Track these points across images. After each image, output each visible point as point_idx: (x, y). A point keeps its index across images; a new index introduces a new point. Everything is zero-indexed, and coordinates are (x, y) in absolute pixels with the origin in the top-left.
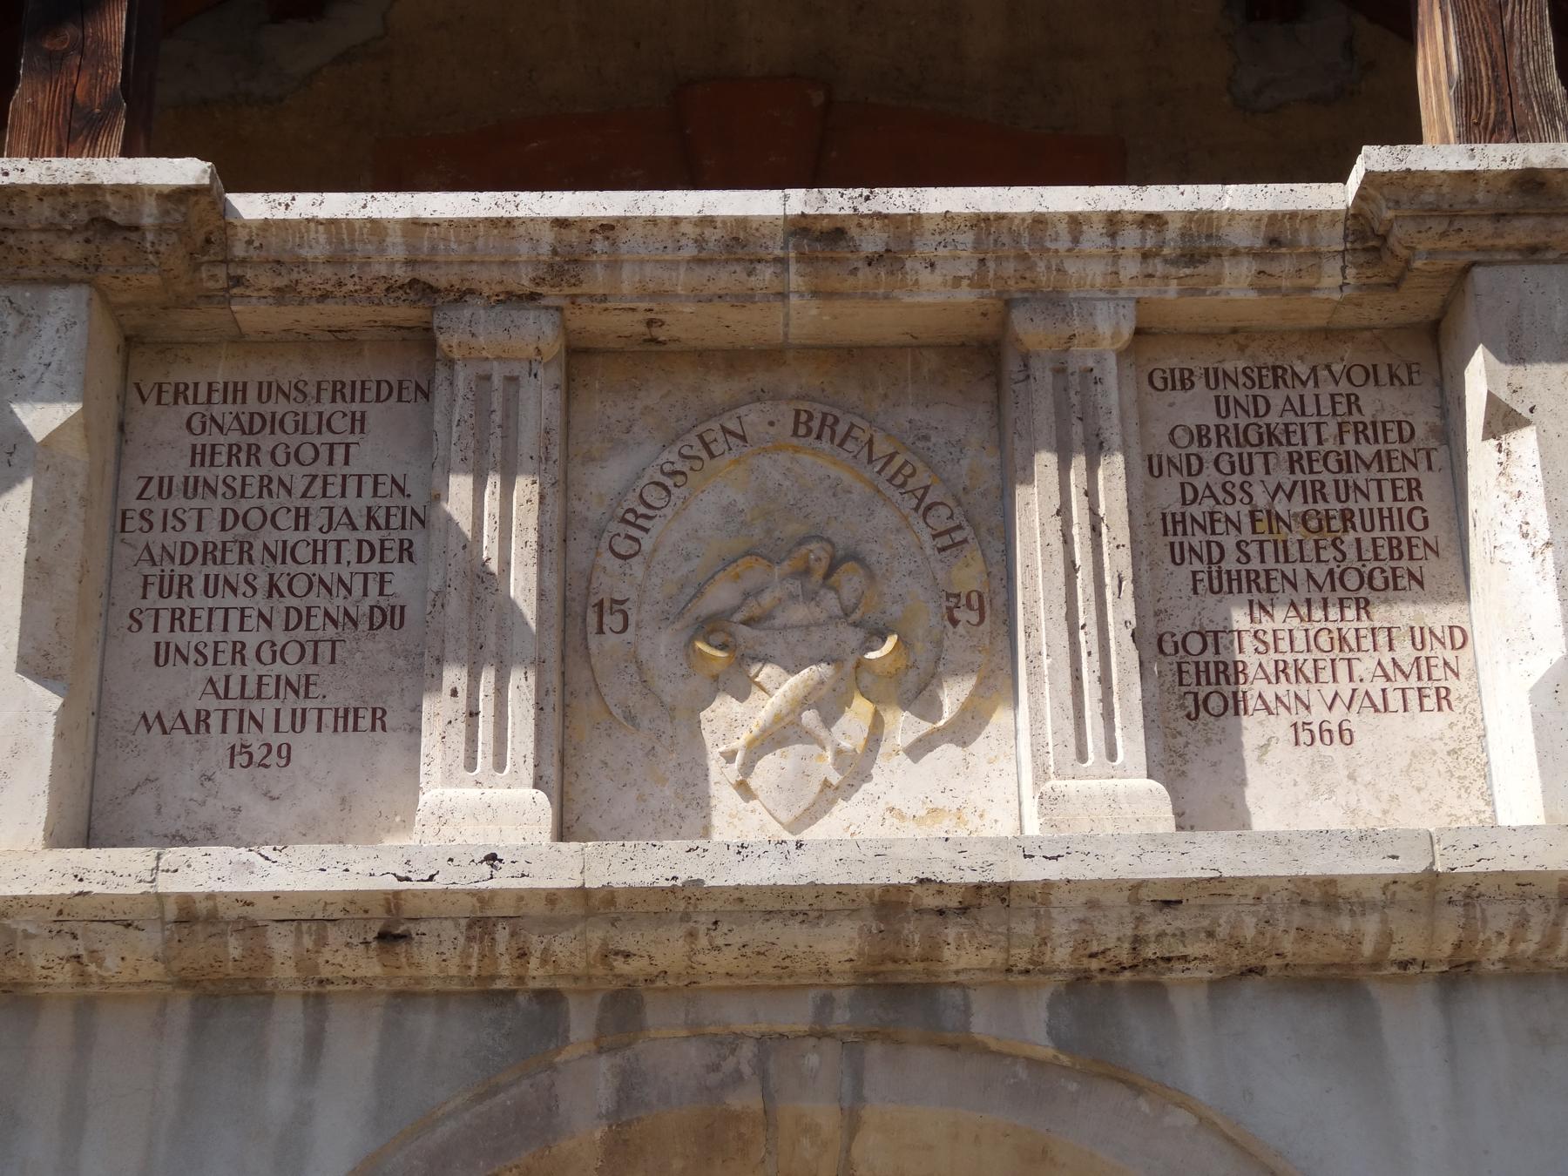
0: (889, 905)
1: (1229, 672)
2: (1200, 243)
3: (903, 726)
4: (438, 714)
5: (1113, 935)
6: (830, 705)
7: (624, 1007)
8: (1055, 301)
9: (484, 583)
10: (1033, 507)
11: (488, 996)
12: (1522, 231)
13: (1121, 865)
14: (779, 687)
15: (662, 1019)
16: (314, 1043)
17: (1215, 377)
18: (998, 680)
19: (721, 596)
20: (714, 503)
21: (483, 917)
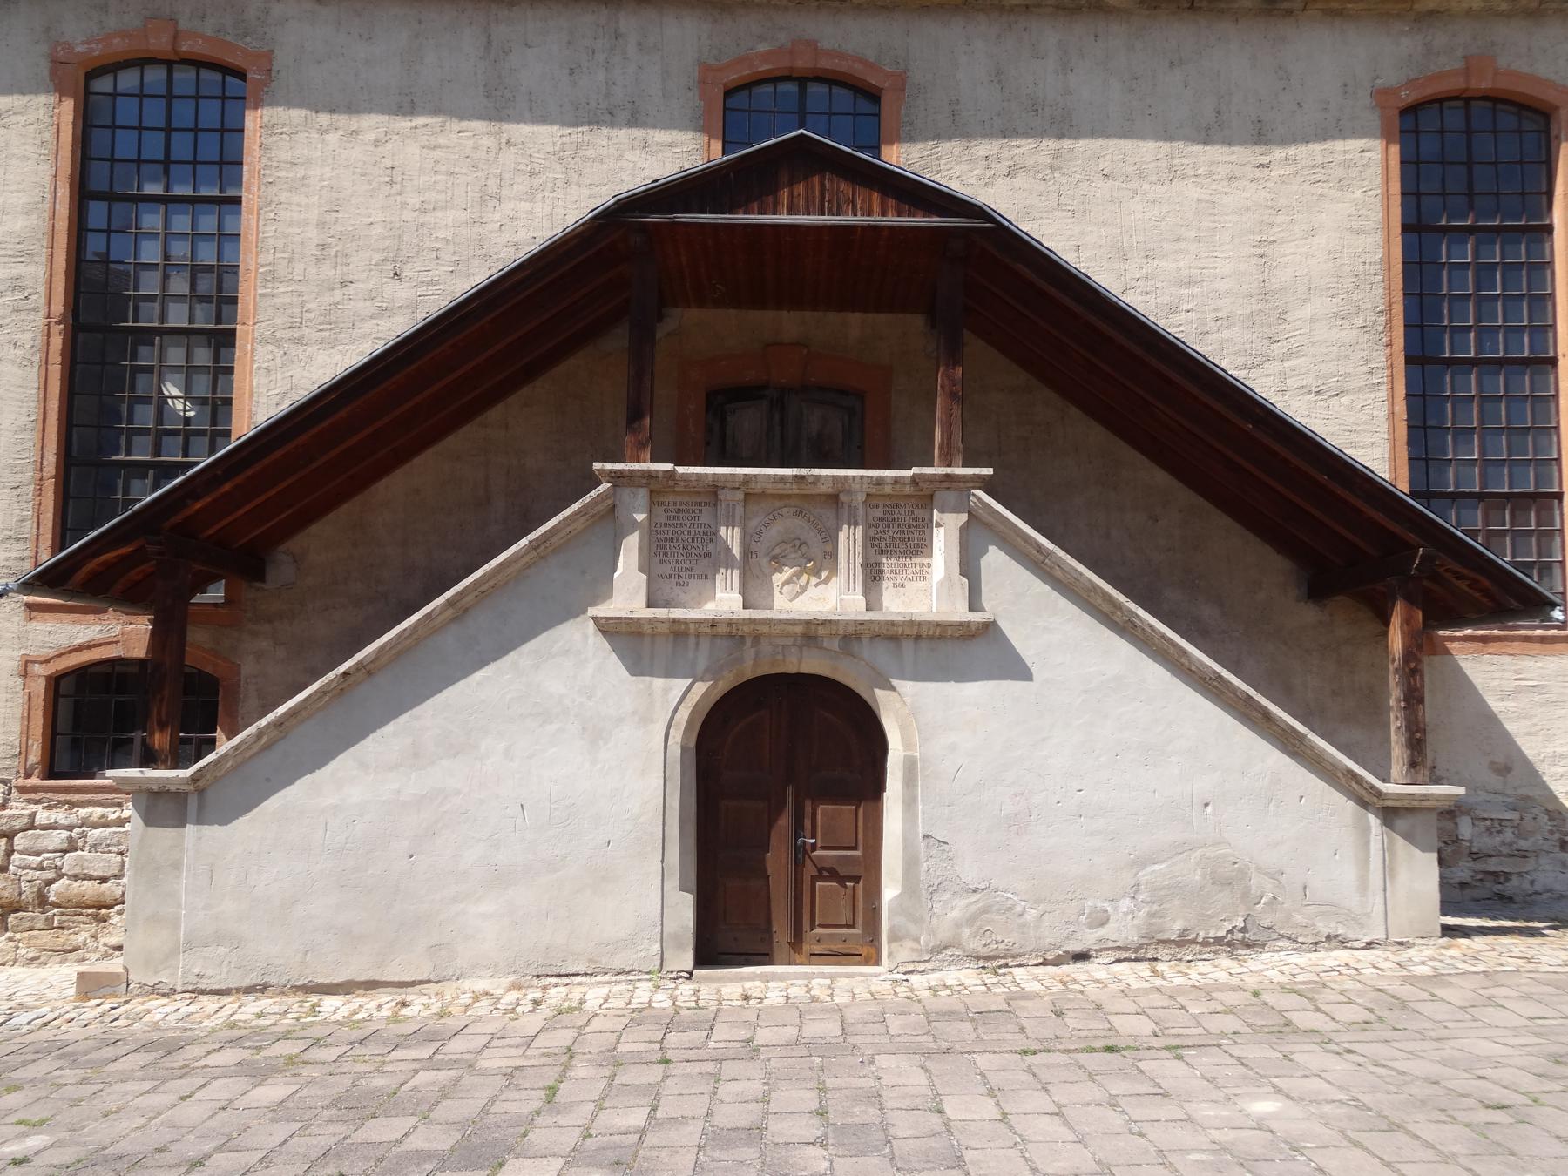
0: (808, 623)
1: (881, 572)
2: (880, 481)
3: (814, 580)
4: (719, 578)
5: (851, 629)
6: (798, 575)
8: (849, 492)
9: (729, 550)
10: (842, 536)
11: (730, 636)
12: (946, 485)
13: (852, 617)
14: (788, 572)
15: (764, 642)
16: (697, 644)
17: (884, 506)
18: (834, 570)
19: (777, 551)
20: (775, 531)
21: (730, 623)
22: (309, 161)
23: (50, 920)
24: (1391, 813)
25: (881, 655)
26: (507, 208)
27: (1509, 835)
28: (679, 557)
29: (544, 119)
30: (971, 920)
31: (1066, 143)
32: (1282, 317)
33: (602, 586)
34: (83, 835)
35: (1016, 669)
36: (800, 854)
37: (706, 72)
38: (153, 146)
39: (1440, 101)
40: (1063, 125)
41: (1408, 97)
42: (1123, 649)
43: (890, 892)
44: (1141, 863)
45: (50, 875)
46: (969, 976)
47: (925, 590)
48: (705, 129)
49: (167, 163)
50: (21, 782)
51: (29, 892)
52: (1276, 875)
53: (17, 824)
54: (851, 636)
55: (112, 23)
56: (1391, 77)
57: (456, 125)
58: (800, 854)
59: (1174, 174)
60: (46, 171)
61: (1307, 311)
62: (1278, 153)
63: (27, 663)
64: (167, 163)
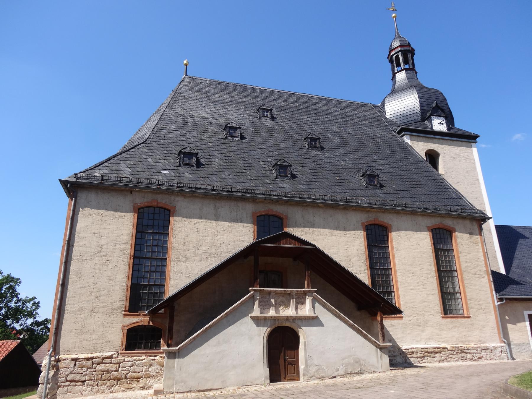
2: (298, 291)
7: (278, 320)
14: (282, 307)
20: (279, 300)
21: (274, 317)
22: (182, 227)
23: (127, 382)
24: (381, 349)
25: (299, 322)
26: (219, 237)
27: (392, 353)
28: (265, 305)
29: (225, 221)
30: (317, 371)
31: (314, 229)
32: (350, 261)
33: (251, 310)
34: (135, 363)
35: (321, 325)
36: (285, 360)
37: (253, 214)
38: (151, 222)
39: (371, 225)
40: (313, 226)
41: (366, 224)
42: (338, 320)
43: (302, 367)
44: (343, 359)
45: (128, 372)
46: (317, 381)
47: (306, 310)
48: (254, 224)
49: (153, 226)
50: (121, 352)
51: (123, 376)
52: (364, 360)
53: (121, 361)
54: (294, 319)
55: (145, 200)
56: (364, 221)
57: (210, 221)
58: (285, 360)
59: (332, 235)
60: (131, 227)
61: (354, 260)
62: (348, 232)
63: (123, 326)
64: (153, 226)
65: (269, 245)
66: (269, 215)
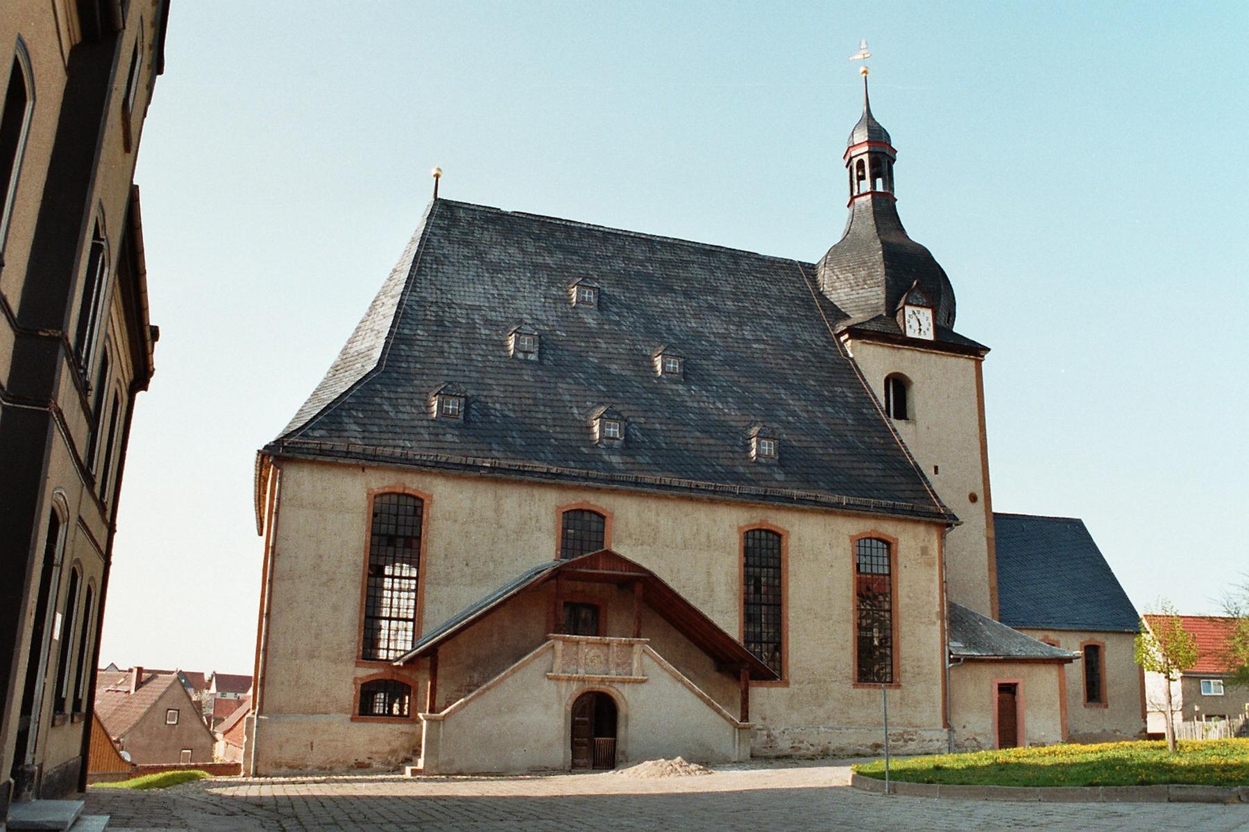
39: (753, 531)
55: (386, 483)
65: (98, 13)
66: (582, 511)
